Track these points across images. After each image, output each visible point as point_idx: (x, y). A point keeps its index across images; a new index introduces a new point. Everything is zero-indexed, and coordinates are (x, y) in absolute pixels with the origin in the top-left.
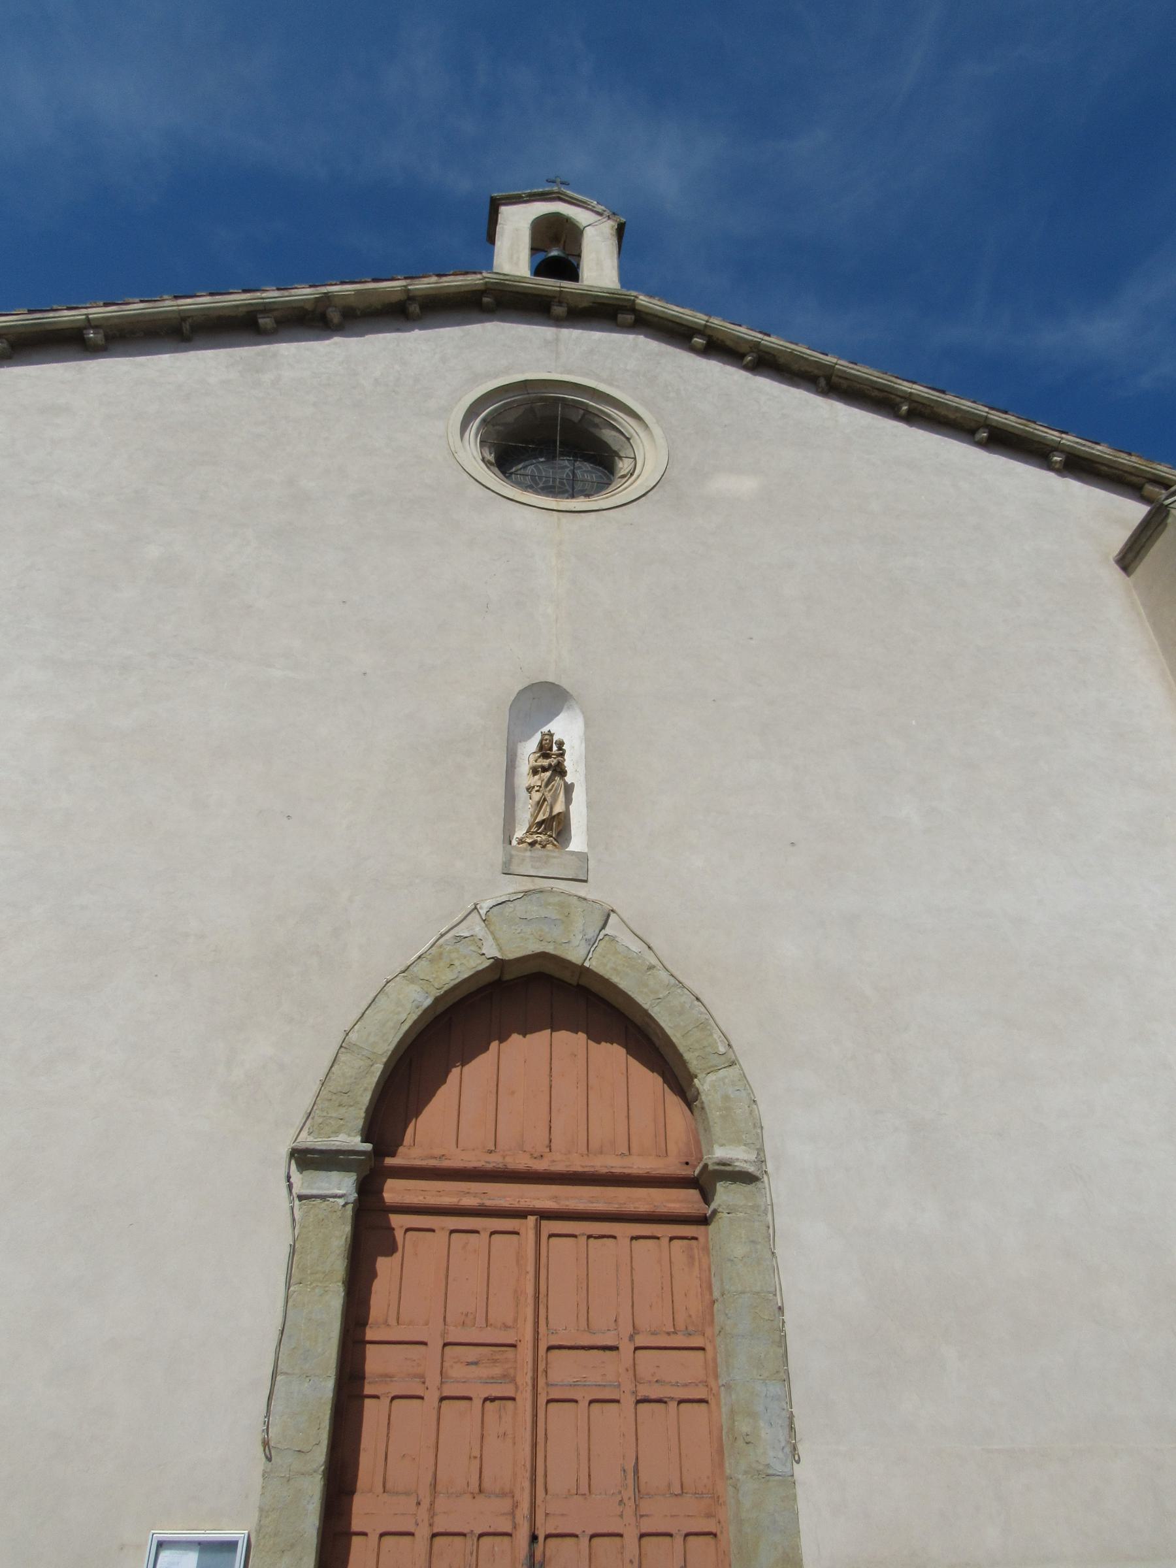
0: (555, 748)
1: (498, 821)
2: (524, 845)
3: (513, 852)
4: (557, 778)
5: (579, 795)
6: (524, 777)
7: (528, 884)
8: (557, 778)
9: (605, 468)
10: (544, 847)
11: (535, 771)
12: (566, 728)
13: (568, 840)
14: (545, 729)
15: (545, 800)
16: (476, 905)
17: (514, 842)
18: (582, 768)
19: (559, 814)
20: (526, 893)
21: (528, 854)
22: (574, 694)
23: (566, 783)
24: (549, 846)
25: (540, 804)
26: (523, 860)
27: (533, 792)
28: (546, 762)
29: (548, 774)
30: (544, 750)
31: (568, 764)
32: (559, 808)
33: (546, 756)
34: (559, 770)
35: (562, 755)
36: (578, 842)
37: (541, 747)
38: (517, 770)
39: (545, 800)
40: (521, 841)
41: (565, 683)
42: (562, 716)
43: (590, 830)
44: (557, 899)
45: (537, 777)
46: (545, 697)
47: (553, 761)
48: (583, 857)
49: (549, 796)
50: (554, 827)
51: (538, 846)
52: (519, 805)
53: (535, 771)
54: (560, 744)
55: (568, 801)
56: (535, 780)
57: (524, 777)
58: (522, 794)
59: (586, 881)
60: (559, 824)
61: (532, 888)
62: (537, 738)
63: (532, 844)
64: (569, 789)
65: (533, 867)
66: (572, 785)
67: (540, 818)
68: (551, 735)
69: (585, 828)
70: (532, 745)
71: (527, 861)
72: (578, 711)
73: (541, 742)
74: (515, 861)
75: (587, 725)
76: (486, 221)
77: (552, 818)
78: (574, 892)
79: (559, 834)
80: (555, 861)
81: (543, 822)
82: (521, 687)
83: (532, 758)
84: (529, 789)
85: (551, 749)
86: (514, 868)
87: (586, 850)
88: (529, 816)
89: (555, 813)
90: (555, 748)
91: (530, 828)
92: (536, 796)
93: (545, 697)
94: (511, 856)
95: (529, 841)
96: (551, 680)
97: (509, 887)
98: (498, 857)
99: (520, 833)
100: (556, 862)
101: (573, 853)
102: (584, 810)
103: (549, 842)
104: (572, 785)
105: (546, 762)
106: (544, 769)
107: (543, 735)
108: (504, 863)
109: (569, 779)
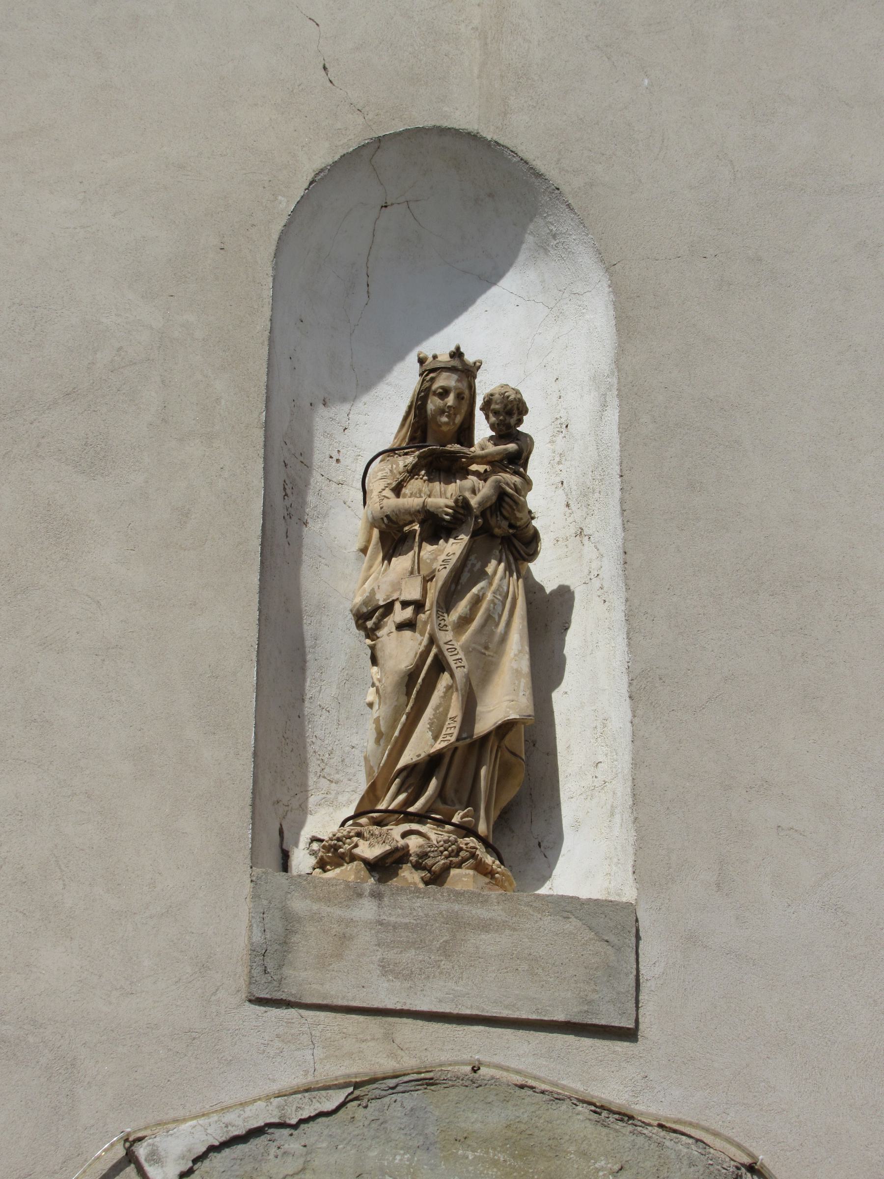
0: (482, 430)
1: (228, 760)
2: (348, 872)
3: (299, 905)
4: (496, 568)
5: (593, 646)
6: (342, 564)
7: (369, 1051)
8: (496, 568)
9: (513, 726)
10: (437, 878)
11: (393, 536)
12: (533, 338)
13: (546, 848)
14: (438, 346)
15: (440, 666)
16: (131, 1143)
17: (303, 860)
18: (606, 524)
19: (505, 728)
20: (359, 1089)
21: (366, 910)
22: (570, 184)
23: (533, 590)
24: (463, 878)
25: (418, 684)
26: (344, 939)
27: (387, 631)
28: (441, 496)
29: (453, 548)
30: (434, 438)
31: (544, 504)
32: (504, 701)
33: (443, 466)
34: (505, 532)
35: (517, 460)
36: (589, 860)
37: (419, 423)
38: (315, 534)
39: (440, 666)
40: (333, 854)
41: (525, 134)
42: (512, 283)
43: (647, 803)
44: (488, 1119)
45: (402, 563)
46: (438, 197)
47: (476, 489)
48: (613, 926)
49: (456, 646)
50: (482, 792)
51: (409, 875)
52: (323, 689)
53: (393, 536)
54: (509, 412)
55: (546, 670)
56: (397, 578)
57: (342, 564)
58: (334, 641)
59: (629, 1034)
60: (504, 773)
61: (387, 1065)
62: (402, 384)
63: (385, 867)
64: (548, 616)
65: (386, 969)
66: (564, 595)
67: (418, 748)
68: (465, 370)
69: (622, 789)
70: (379, 417)
71: (362, 944)
72: (586, 259)
73: (419, 405)
74: (308, 945)
75: (626, 324)
76: (399, 424)
77: (473, 748)
78: (574, 1084)
79: (504, 820)
80: (489, 943)
81: (432, 764)
82: (323, 156)
83: (382, 476)
84: (369, 618)
85: (465, 434)
86: (304, 978)
87: (629, 894)
88: (418, 903)
89: (485, 724)
90: (482, 430)
91: (373, 793)
92: (401, 650)
93: (438, 197)
94: (291, 923)
95: (369, 850)
96: (463, 117)
97: (278, 1063)
98: (229, 923)
99: (326, 818)
100: (486, 949)
101: (568, 906)
102: (619, 715)
103: (457, 858)
104: (564, 595)
105: (441, 496)
106: (436, 527)
107: (429, 370)
108: (260, 955)
109: (546, 570)
